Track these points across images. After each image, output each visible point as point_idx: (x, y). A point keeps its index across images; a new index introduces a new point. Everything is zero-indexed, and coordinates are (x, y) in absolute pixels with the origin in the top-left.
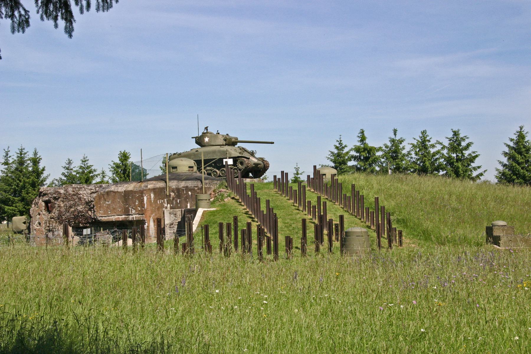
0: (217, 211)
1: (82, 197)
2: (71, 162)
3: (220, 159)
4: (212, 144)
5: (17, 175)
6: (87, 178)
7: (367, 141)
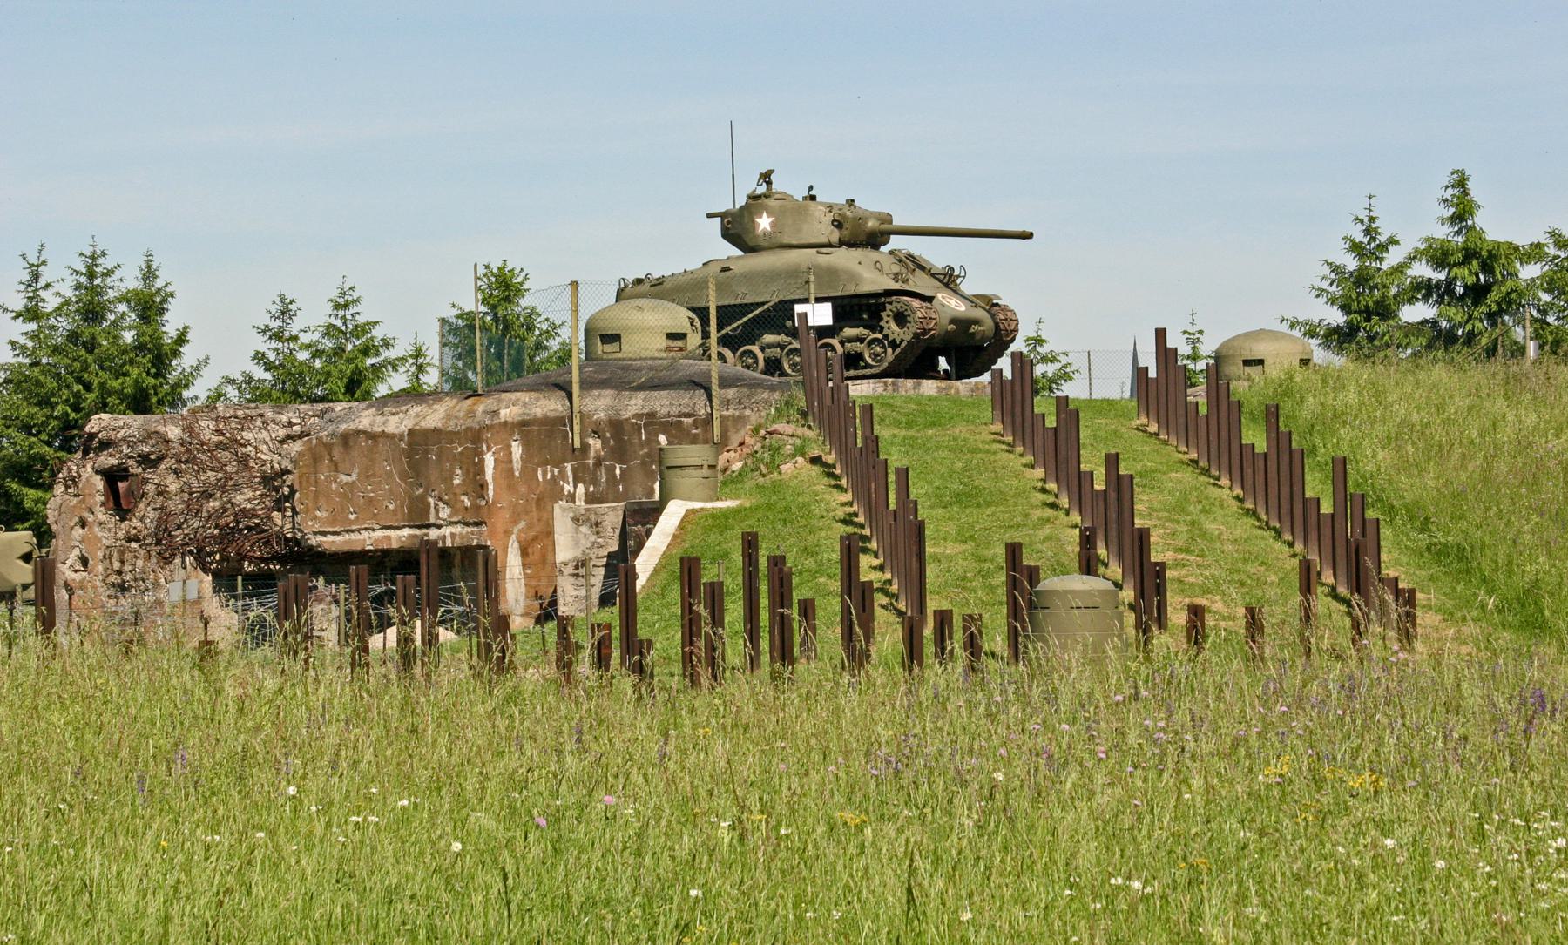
0: (736, 511)
1: (253, 453)
2: (291, 307)
3: (781, 302)
4: (786, 240)
5: (74, 360)
6: (353, 373)
7: (1480, 220)
